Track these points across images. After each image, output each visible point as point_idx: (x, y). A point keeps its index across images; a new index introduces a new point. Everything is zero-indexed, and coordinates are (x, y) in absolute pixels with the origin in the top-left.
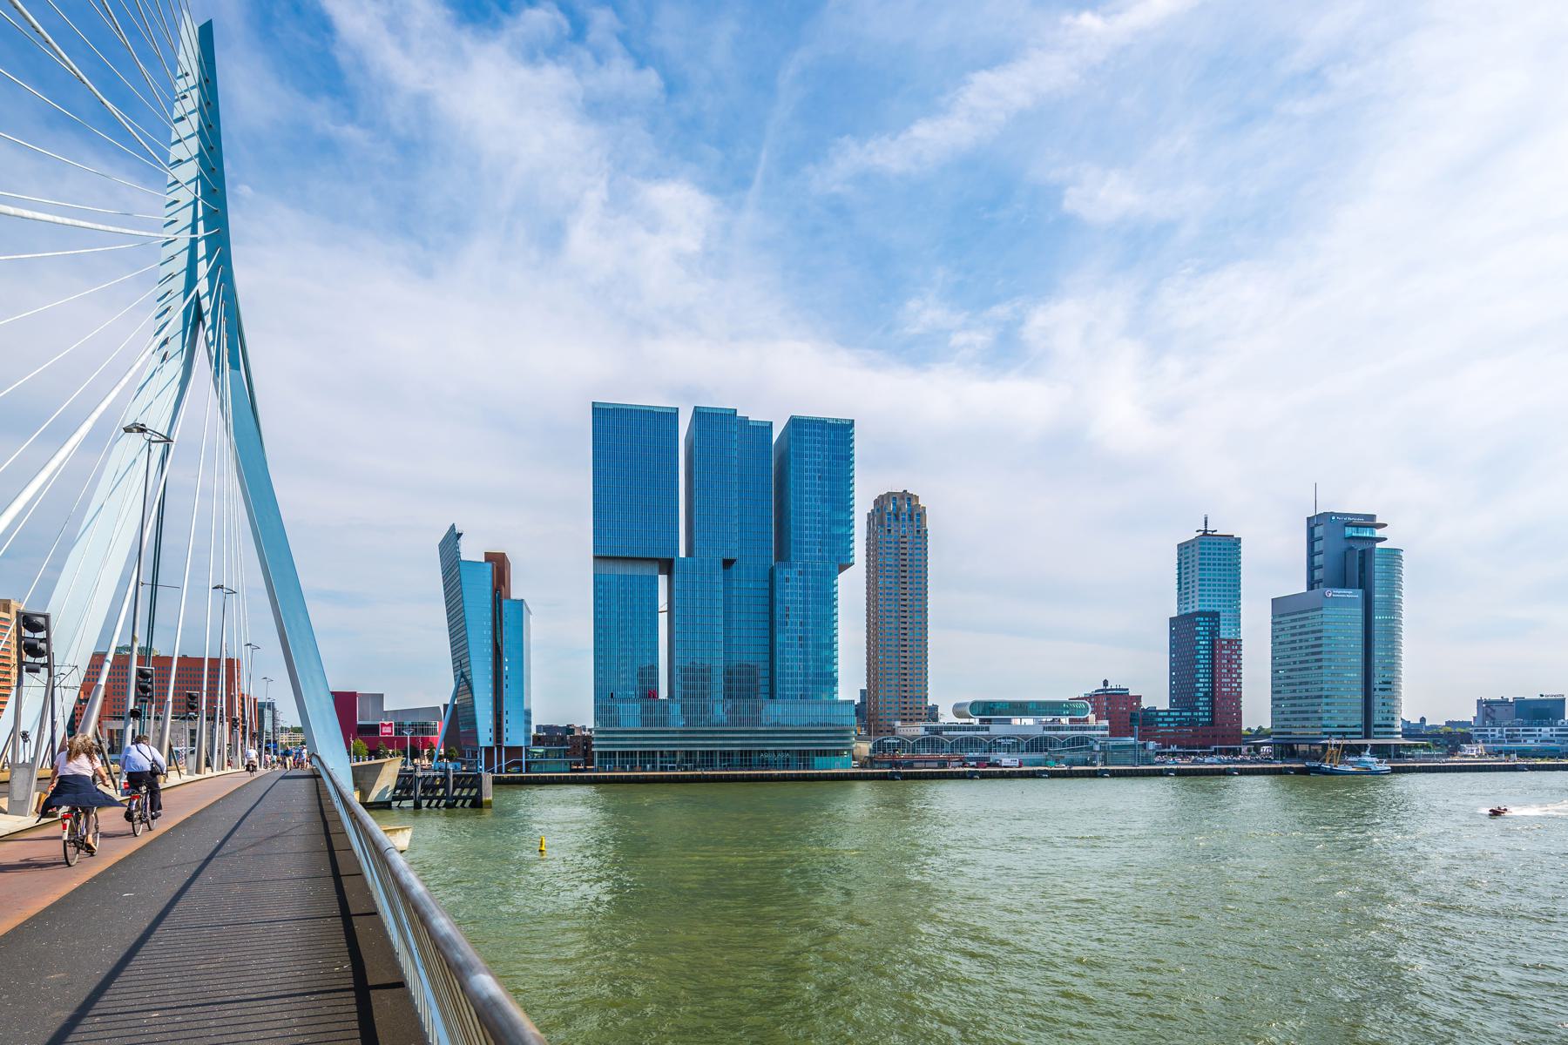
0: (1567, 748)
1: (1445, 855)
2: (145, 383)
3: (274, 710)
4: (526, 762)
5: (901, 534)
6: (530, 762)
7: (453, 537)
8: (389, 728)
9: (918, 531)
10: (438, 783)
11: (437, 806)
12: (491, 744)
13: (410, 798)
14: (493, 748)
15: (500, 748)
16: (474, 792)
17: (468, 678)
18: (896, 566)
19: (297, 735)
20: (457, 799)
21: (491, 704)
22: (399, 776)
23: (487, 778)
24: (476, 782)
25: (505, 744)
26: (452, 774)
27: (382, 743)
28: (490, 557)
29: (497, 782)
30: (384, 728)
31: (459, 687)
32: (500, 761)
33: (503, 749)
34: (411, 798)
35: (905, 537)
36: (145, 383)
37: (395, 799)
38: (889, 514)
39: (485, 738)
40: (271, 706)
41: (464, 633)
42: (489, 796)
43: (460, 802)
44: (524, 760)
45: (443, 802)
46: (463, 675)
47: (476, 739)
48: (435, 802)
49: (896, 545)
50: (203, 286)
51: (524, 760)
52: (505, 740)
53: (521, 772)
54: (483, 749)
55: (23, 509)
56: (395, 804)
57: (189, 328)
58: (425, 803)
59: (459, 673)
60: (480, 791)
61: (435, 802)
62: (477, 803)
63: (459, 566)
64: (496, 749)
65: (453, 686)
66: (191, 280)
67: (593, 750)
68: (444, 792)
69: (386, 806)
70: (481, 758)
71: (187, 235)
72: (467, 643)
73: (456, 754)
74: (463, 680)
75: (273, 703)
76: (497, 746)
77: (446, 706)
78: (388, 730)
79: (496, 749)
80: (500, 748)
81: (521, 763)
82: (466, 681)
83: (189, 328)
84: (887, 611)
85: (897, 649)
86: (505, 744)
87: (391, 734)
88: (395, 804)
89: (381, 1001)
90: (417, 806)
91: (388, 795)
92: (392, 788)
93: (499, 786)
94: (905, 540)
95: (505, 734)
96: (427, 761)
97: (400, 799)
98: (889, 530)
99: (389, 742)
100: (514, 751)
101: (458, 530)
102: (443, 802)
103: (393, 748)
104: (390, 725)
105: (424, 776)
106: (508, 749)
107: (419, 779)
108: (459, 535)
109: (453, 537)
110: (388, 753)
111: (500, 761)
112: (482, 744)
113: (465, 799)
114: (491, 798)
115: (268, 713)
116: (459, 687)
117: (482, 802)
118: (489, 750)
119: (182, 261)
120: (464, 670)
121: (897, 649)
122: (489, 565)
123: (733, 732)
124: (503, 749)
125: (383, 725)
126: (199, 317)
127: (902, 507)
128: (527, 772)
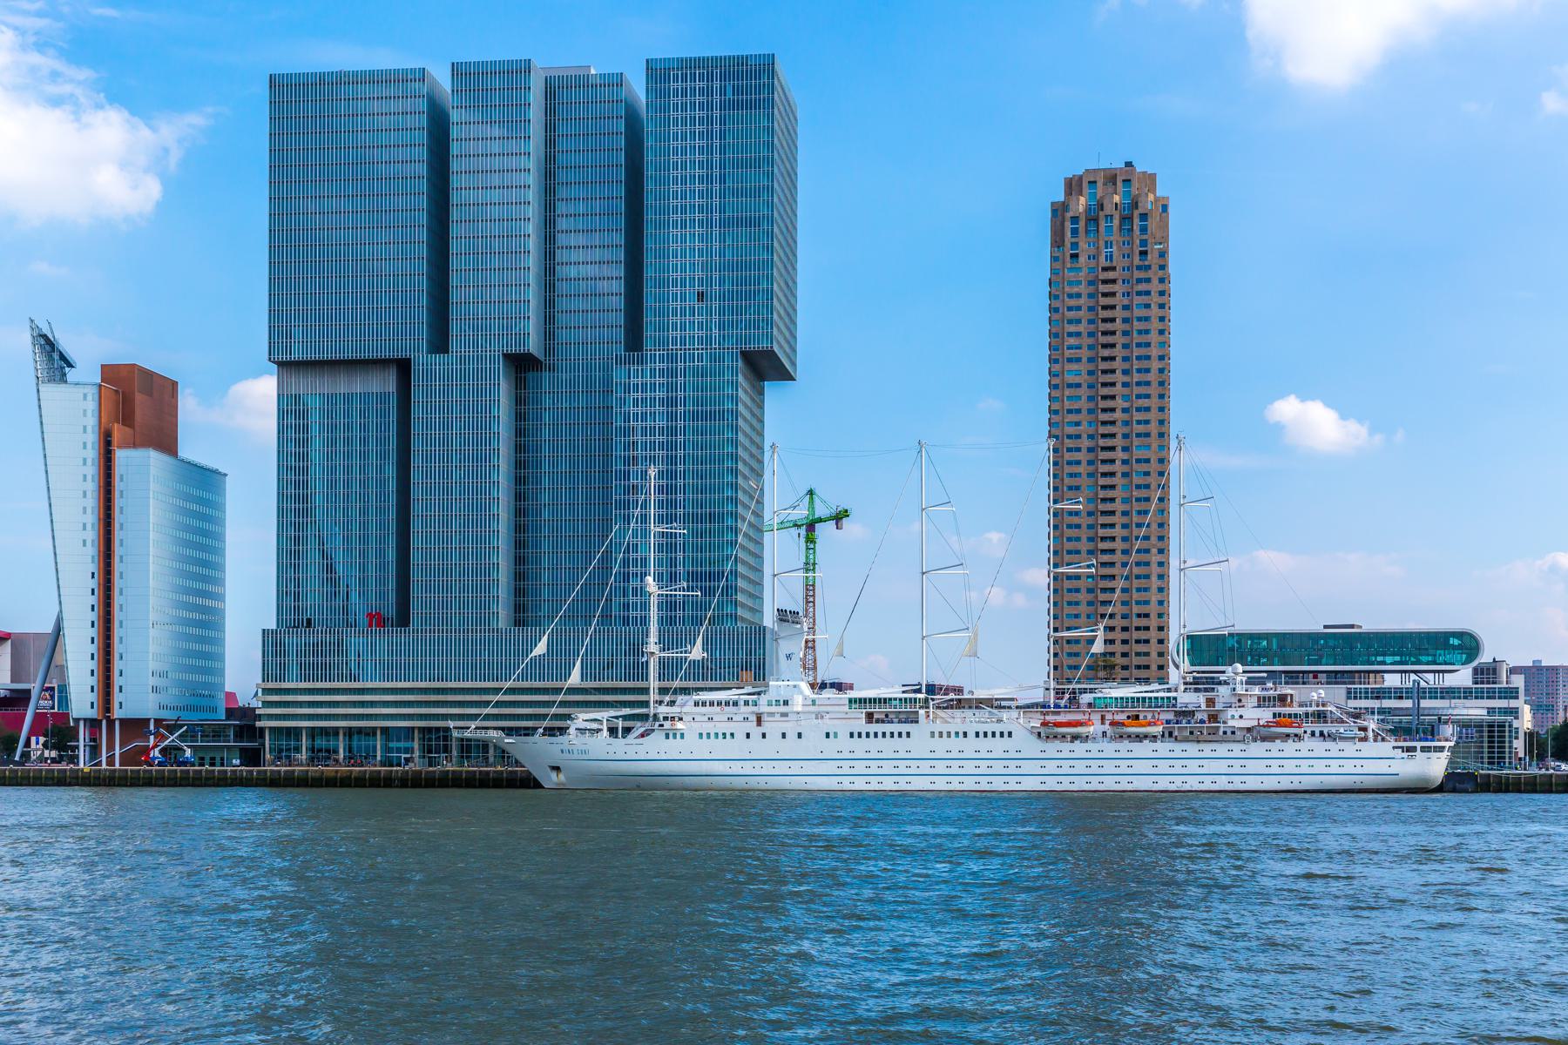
1: (1322, 855)
5: (1103, 262)
9: (1144, 253)
12: (92, 714)
14: (101, 721)
15: (111, 723)
18: (1091, 334)
25: (117, 713)
32: (111, 747)
35: (1114, 269)
38: (1075, 220)
49: (1092, 288)
52: (116, 706)
55: (241, 380)
64: (104, 722)
67: (258, 724)
79: (104, 722)
80: (111, 723)
84: (1069, 437)
85: (1091, 520)
86: (117, 713)
87: (53, 708)
94: (1111, 275)
95: (117, 697)
98: (1075, 256)
99: (1275, 654)
100: (134, 726)
106: (122, 721)
111: (111, 747)
118: (93, 724)
121: (1091, 520)
123: (624, 691)
127: (1142, 199)
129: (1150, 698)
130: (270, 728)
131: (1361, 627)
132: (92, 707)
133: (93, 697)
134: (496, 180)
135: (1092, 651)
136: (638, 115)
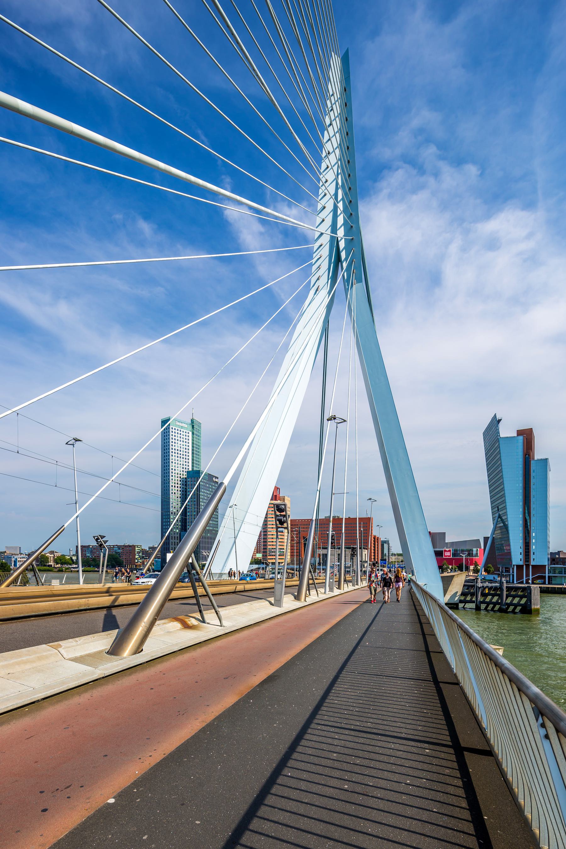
0: (565, 588)
2: (308, 307)
3: (388, 544)
4: (549, 577)
6: (551, 576)
7: (496, 422)
8: (449, 553)
10: (487, 592)
11: (492, 609)
12: (521, 563)
13: (471, 602)
15: (527, 566)
16: (523, 601)
17: (504, 518)
19: (399, 557)
20: (509, 605)
21: (521, 535)
22: (464, 586)
23: (535, 588)
24: (527, 593)
25: (532, 563)
26: (505, 585)
27: (445, 562)
28: (520, 433)
29: (543, 591)
30: (446, 553)
31: (496, 528)
32: (527, 575)
33: (531, 567)
34: (473, 602)
36: (308, 307)
37: (461, 601)
39: (517, 558)
40: (387, 542)
41: (502, 486)
42: (537, 605)
43: (511, 608)
44: (547, 575)
45: (497, 607)
46: (500, 517)
47: (510, 560)
48: (491, 606)
50: (341, 233)
51: (547, 575)
53: (544, 583)
54: (515, 567)
56: (461, 605)
57: (332, 265)
58: (483, 606)
59: (497, 515)
60: (529, 600)
61: (491, 606)
62: (527, 610)
63: (499, 441)
64: (525, 567)
65: (492, 526)
66: (334, 228)
68: (498, 600)
69: (455, 606)
70: (513, 572)
71: (332, 202)
72: (504, 494)
73: (492, 569)
74: (499, 519)
75: (388, 541)
76: (526, 565)
77: (486, 539)
78: (447, 554)
79: (525, 567)
80: (527, 566)
81: (545, 577)
82: (502, 520)
83: (332, 265)
86: (532, 563)
87: (450, 556)
88: (461, 605)
89: (429, 639)
90: (478, 608)
91: (457, 598)
92: (459, 593)
93: (545, 595)
95: (532, 557)
96: (471, 573)
97: (465, 602)
99: (450, 561)
100: (539, 568)
101: (498, 417)
102: (519, 608)
103: (452, 565)
104: (450, 551)
105: (483, 587)
106: (532, 566)
107: (479, 588)
108: (499, 421)
109: (496, 422)
110: (449, 568)
111: (527, 575)
112: (514, 563)
113: (516, 606)
114: (538, 607)
115: (386, 546)
116: (497, 522)
117: (531, 609)
118: (519, 567)
119: (329, 221)
120: (501, 513)
122: (521, 438)
124: (531, 567)
125: (445, 551)
126: (338, 259)
128: (549, 583)
129: (291, 528)
130: (548, 574)
131: (8, 586)
132: (521, 560)
133: (521, 557)
134: (420, 728)
135: (155, 579)
136: (537, 693)
